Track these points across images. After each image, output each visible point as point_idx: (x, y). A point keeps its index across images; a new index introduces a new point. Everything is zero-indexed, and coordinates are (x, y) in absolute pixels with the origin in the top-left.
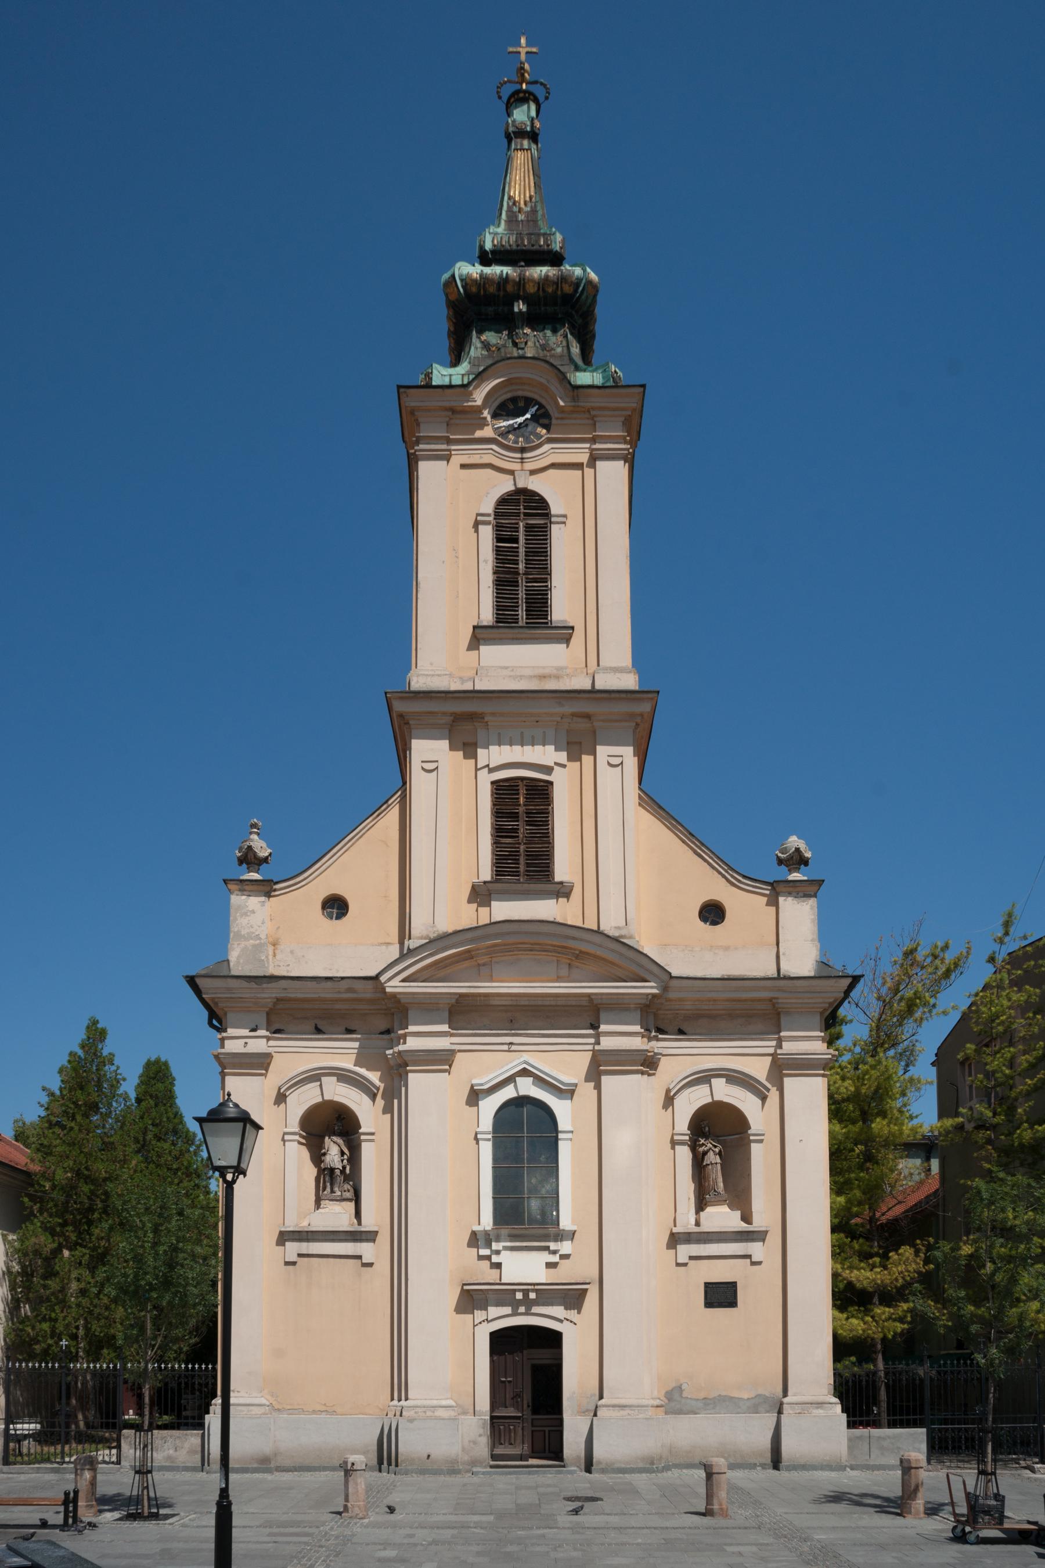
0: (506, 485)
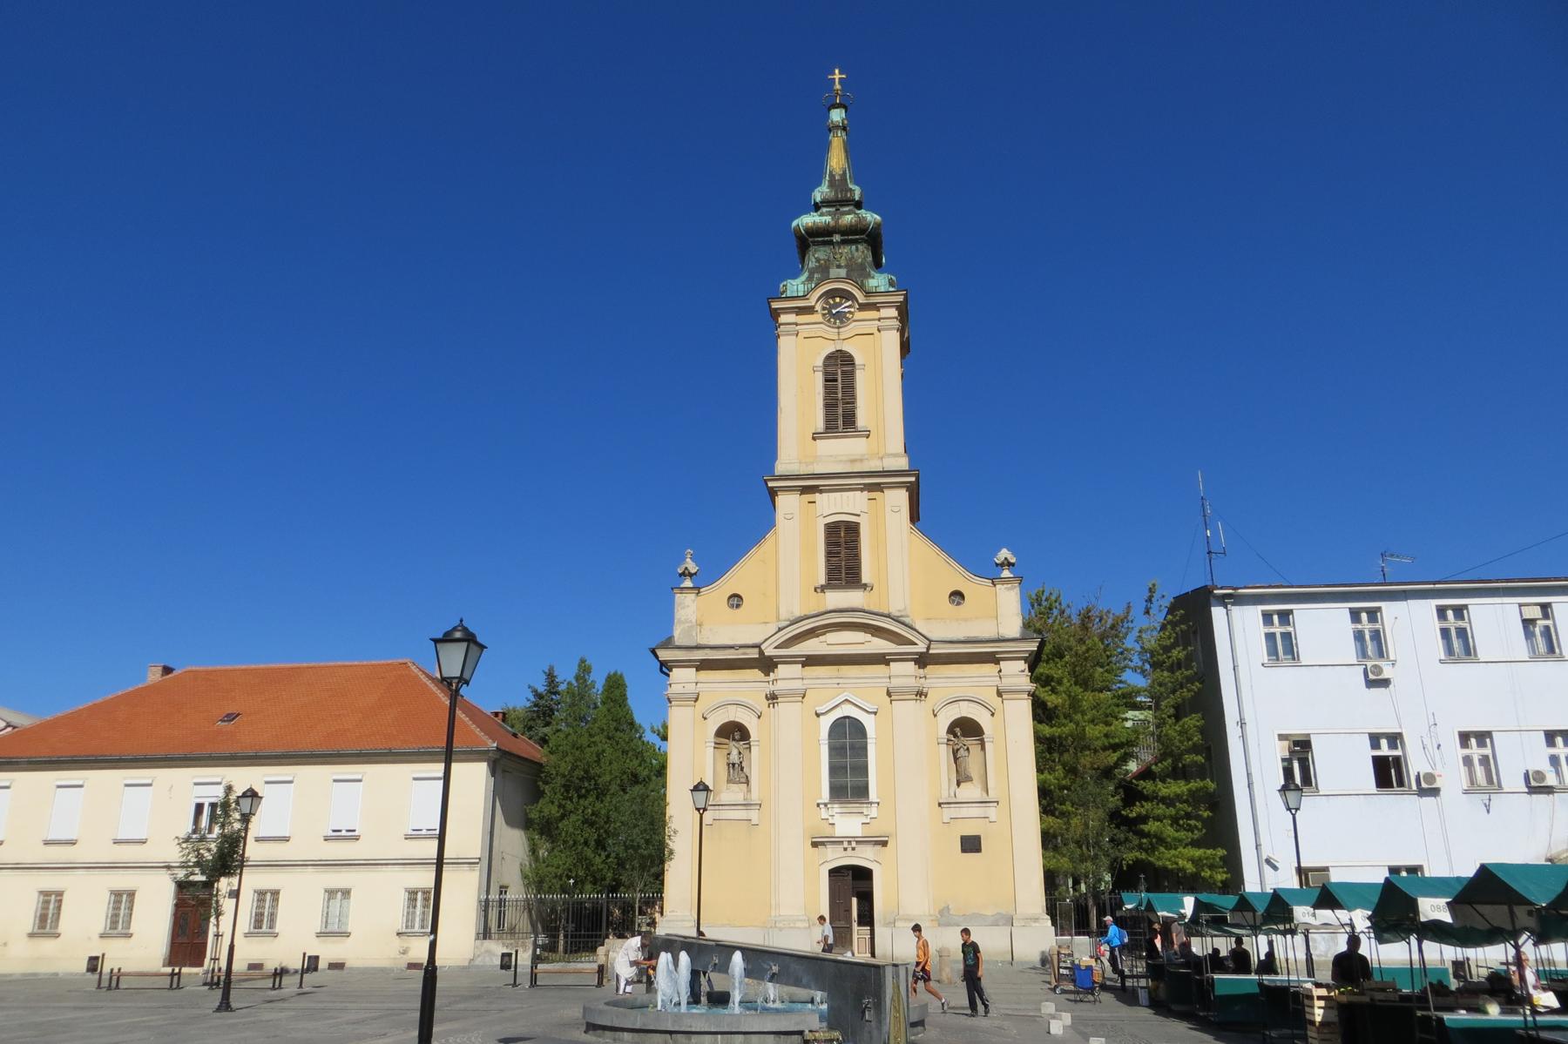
0: (831, 348)
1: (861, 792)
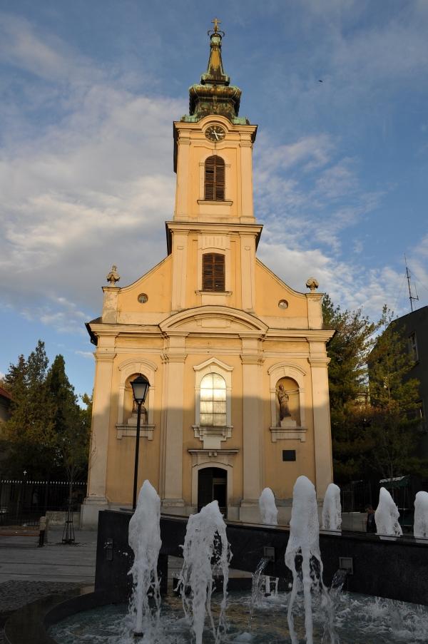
0: (210, 154)
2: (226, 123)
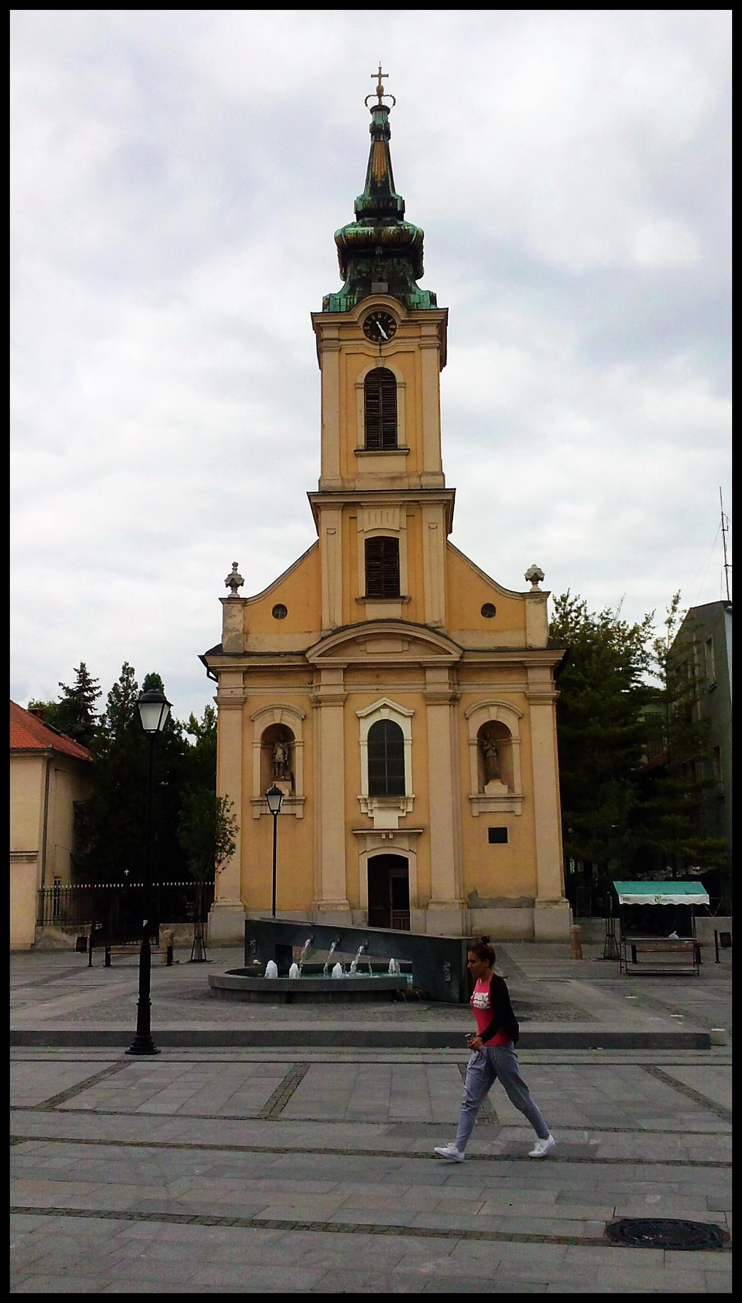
1: (398, 789)
2: (398, 308)
